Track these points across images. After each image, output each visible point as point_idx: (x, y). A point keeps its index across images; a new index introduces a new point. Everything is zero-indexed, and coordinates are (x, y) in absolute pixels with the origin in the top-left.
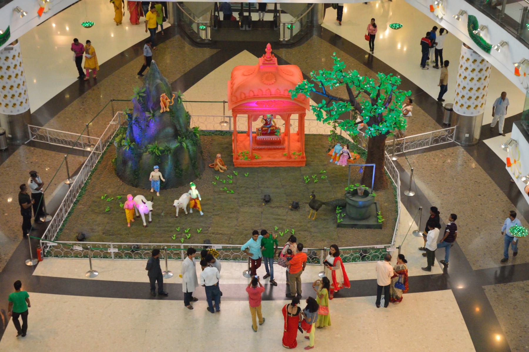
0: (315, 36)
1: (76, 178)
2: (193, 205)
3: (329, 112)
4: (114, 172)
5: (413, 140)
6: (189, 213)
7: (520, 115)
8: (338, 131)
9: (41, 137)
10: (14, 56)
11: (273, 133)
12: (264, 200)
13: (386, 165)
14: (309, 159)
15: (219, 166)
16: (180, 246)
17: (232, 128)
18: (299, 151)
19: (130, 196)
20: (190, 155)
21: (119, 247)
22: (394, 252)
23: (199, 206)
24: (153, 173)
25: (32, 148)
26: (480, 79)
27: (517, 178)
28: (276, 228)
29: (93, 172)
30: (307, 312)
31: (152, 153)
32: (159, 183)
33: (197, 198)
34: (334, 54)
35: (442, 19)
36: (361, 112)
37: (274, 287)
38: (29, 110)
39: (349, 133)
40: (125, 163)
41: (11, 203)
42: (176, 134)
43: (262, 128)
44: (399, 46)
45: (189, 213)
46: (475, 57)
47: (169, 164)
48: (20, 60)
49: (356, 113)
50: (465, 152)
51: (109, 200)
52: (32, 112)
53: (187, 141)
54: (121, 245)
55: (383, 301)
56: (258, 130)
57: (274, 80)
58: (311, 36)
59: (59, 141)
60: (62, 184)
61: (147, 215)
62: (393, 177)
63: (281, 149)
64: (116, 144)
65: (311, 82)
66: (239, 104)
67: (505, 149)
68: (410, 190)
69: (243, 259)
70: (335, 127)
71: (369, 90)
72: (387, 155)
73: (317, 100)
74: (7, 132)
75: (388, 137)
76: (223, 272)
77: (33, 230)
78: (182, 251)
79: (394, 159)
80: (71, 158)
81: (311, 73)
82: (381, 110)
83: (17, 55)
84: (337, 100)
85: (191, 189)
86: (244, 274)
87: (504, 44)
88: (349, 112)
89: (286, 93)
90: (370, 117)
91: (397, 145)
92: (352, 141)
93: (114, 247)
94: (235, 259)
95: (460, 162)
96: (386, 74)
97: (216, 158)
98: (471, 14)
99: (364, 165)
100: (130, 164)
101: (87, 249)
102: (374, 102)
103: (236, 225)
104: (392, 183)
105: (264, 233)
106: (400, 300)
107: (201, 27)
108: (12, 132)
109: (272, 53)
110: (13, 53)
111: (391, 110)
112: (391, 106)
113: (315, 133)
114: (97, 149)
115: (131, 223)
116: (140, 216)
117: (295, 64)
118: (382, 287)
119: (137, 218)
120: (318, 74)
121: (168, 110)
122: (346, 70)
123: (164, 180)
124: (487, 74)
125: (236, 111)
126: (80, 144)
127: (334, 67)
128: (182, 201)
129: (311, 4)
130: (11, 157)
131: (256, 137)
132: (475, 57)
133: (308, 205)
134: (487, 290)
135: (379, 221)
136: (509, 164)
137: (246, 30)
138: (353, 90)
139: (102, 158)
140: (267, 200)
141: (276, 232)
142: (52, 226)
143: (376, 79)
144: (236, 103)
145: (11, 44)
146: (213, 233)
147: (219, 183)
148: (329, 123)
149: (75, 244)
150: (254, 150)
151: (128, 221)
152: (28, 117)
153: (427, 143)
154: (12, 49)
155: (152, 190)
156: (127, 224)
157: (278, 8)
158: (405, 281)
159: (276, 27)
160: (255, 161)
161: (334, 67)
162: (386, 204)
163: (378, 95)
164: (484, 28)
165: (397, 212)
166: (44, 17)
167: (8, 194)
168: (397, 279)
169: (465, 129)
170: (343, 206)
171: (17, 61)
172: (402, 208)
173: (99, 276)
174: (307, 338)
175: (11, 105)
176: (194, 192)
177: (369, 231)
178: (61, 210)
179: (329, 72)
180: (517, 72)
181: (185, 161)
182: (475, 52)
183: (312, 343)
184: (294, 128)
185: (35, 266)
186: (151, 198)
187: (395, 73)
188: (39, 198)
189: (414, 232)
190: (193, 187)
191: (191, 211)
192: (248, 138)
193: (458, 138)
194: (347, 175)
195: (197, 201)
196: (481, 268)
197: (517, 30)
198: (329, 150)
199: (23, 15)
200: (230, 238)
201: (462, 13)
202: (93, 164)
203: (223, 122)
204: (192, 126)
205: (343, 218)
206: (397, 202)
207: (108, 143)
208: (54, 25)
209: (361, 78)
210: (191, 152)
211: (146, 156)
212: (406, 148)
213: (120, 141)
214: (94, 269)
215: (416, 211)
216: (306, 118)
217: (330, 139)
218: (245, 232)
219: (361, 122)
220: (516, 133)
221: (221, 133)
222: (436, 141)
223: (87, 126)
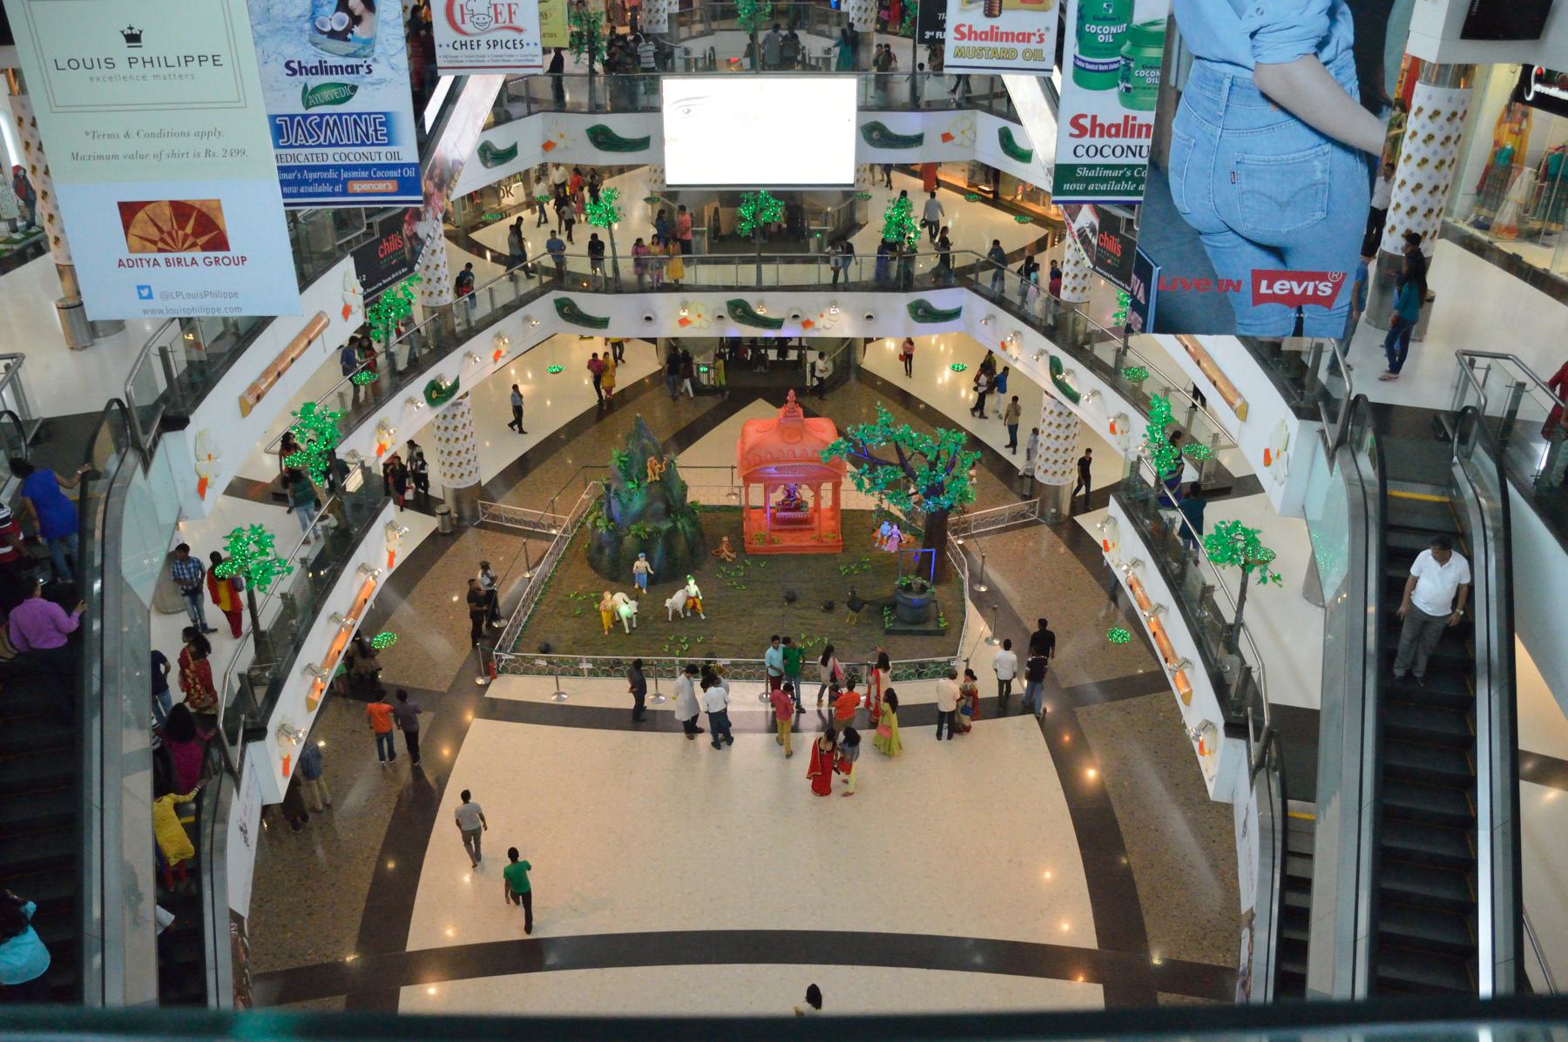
0: (853, 380)
1: (538, 569)
2: (691, 605)
3: (872, 480)
4: (587, 563)
5: (984, 517)
6: (686, 616)
7: (1118, 484)
8: (885, 505)
9: (494, 517)
10: (463, 413)
11: (798, 508)
12: (787, 598)
13: (949, 550)
14: (847, 543)
15: (726, 552)
16: (673, 661)
17: (743, 503)
18: (833, 532)
19: (607, 595)
20: (687, 540)
21: (594, 662)
22: (961, 668)
23: (699, 606)
24: (637, 563)
25: (483, 531)
26: (1067, 437)
27: (1117, 566)
28: (803, 636)
29: (559, 562)
30: (846, 747)
31: (637, 536)
32: (645, 576)
33: (697, 597)
34: (879, 404)
35: (1017, 359)
36: (915, 480)
37: (802, 715)
38: (480, 482)
39: (899, 507)
40: (600, 549)
41: (457, 602)
42: (669, 511)
43: (783, 501)
44: (963, 393)
45: (686, 616)
46: (1060, 409)
47: (658, 552)
48: (470, 417)
49: (909, 481)
50: (1051, 533)
51: (580, 598)
52: (483, 484)
53: (683, 520)
54: (596, 660)
55: (945, 732)
56: (778, 504)
57: (799, 438)
58: (848, 379)
59: (516, 521)
60: (520, 578)
61: (629, 620)
62: (959, 567)
63: (809, 529)
64: (589, 526)
65: (847, 439)
66: (751, 470)
67: (1102, 529)
68: (981, 583)
69: (760, 678)
70: (881, 500)
71: (925, 450)
72: (951, 537)
73: (856, 464)
74: (452, 511)
75: (952, 512)
76: (731, 696)
77: (485, 637)
78: (677, 668)
79: (960, 542)
80: (531, 543)
81: (849, 429)
82: (943, 477)
83: (466, 411)
84: (883, 463)
85: (688, 584)
86: (761, 697)
87: (1095, 393)
88: (899, 480)
89: (816, 455)
90: (927, 486)
91: (963, 523)
92: (904, 518)
93: (588, 662)
94: (748, 678)
95: (1045, 545)
96: (948, 429)
97: (722, 542)
98: (1053, 354)
99: (920, 550)
100: (607, 551)
101: (552, 663)
102: (932, 466)
103: (749, 632)
104: (957, 574)
105: (786, 641)
106: (967, 729)
107: (702, 369)
108: (459, 511)
109: (796, 402)
110: (462, 408)
111: (955, 478)
112: (955, 471)
113: (854, 508)
114: (564, 532)
115: (610, 631)
116: (620, 621)
117: (828, 416)
118: (944, 713)
119: (617, 623)
120: (857, 430)
121: (658, 479)
122: (895, 425)
123: (652, 572)
124: (1076, 431)
125: (748, 480)
126: (544, 526)
127: (879, 421)
128: (677, 600)
129: (848, 339)
130: (457, 543)
131: (774, 514)
132: (1060, 409)
133: (845, 605)
134: (1079, 714)
135: (941, 625)
136: (1107, 549)
137: (761, 373)
138: (903, 450)
139: (571, 543)
140: (791, 599)
141: (803, 641)
142: (508, 633)
143: (935, 436)
144: (748, 469)
145: (461, 398)
146: (718, 644)
147: (726, 575)
148: (873, 495)
149: (537, 657)
150: (774, 530)
151: (606, 627)
152: (481, 491)
153: (1002, 521)
154: (461, 404)
155: (636, 586)
156: (604, 631)
157: (804, 344)
158: (974, 704)
159: (801, 367)
160: (773, 546)
161: (879, 421)
162: (950, 603)
163: (938, 457)
164: (1070, 372)
165: (964, 613)
166: (501, 362)
167: (453, 591)
168: (964, 701)
169: (1050, 502)
170: (893, 606)
171: (465, 420)
172: (970, 608)
173: (569, 700)
174: (846, 782)
175: (457, 475)
176: (693, 588)
177: (927, 639)
178: (519, 611)
179: (873, 427)
180: (1112, 428)
181: (681, 546)
182: (1059, 402)
183: (851, 788)
184: (826, 503)
185: (486, 686)
186: (635, 595)
187: (959, 428)
188: (491, 597)
189: (987, 640)
190: (692, 582)
191: (689, 614)
192: (764, 515)
193: (1042, 514)
194: (897, 564)
195: (697, 601)
196: (1071, 685)
197: (1110, 376)
198: (874, 531)
199: (476, 361)
200: (741, 650)
201: (1042, 352)
202: (559, 551)
203: (729, 494)
204: (689, 500)
205: (893, 622)
206: (964, 600)
207: (579, 524)
208: (513, 372)
209: (915, 435)
210: (689, 535)
211: (628, 540)
212: (976, 527)
213: (595, 521)
214: (561, 690)
215: (989, 611)
216: (842, 487)
217: (874, 516)
218: (761, 642)
219: (916, 493)
220: (1114, 508)
221: (728, 509)
222: (1014, 518)
223: (552, 501)
